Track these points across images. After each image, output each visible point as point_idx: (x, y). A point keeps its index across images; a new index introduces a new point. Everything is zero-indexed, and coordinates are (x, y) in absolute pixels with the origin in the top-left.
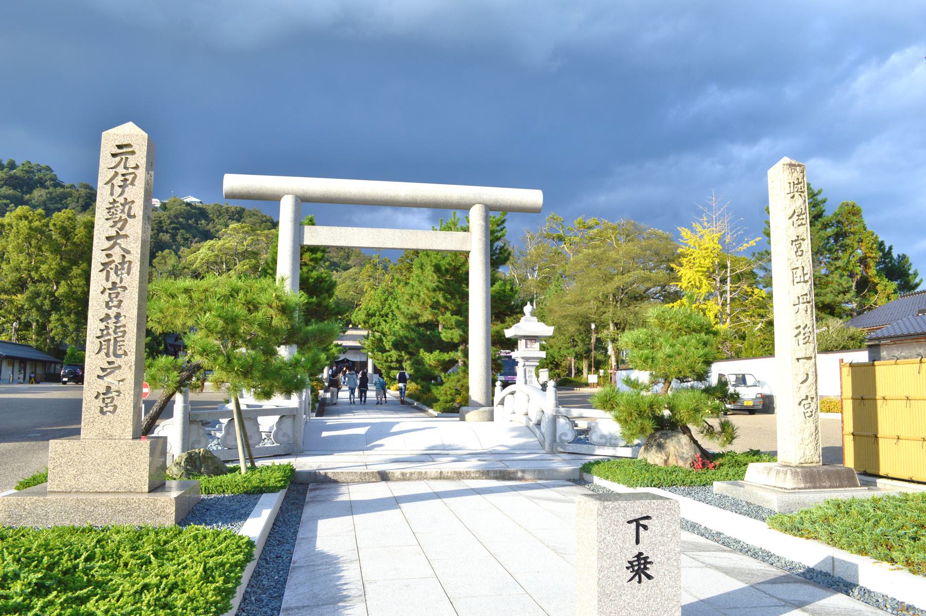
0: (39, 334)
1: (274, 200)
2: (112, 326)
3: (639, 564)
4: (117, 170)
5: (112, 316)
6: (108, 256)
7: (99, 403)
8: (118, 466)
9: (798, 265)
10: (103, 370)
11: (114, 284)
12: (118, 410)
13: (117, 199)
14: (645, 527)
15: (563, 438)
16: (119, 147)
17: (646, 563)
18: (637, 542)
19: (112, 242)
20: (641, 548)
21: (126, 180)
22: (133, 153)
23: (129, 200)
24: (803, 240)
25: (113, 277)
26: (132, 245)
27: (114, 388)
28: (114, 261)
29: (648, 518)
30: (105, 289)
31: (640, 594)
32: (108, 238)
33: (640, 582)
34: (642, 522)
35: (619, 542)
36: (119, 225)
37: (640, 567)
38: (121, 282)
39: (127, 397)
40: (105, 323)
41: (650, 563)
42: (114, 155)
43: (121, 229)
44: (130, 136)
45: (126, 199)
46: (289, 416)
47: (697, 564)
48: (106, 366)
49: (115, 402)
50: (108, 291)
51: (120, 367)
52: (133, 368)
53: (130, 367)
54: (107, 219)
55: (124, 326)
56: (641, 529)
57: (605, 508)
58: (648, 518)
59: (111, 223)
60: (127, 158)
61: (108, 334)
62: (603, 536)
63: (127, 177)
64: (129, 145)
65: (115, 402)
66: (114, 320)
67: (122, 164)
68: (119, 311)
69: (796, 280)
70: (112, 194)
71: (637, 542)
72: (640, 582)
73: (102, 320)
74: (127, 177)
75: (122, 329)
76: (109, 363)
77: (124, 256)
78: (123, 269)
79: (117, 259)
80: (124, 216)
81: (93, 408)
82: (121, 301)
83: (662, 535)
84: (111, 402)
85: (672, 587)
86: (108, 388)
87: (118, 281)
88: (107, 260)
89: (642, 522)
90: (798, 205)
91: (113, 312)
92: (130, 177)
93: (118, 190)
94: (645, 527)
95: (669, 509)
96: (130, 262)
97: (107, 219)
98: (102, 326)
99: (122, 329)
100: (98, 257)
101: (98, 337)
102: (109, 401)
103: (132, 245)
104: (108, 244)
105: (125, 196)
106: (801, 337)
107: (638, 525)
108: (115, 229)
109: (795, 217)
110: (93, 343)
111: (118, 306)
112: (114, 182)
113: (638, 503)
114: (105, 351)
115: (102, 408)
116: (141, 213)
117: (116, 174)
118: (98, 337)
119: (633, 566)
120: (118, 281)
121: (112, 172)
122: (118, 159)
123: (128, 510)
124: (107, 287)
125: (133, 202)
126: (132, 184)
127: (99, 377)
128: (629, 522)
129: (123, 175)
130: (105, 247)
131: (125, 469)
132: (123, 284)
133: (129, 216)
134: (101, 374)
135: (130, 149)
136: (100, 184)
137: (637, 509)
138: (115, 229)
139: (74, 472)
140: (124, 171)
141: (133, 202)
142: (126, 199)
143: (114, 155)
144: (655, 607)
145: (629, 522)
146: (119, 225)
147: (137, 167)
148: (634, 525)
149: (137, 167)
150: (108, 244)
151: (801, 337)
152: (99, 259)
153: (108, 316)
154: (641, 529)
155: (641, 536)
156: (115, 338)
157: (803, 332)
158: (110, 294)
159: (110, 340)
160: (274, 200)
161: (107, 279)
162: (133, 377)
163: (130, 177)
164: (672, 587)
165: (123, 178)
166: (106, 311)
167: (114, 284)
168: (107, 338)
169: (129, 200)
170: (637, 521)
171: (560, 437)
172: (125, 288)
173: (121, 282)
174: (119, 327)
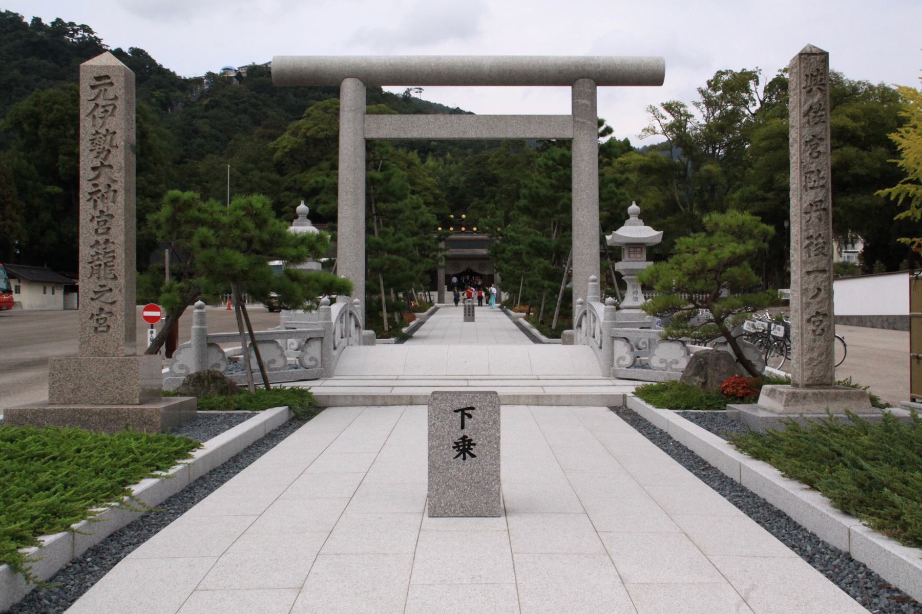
3: (464, 445)
5: (102, 242)
6: (95, 185)
8: (111, 380)
9: (813, 167)
10: (95, 292)
12: (111, 330)
13: (100, 131)
14: (470, 416)
15: (621, 362)
16: (98, 78)
17: (470, 444)
18: (463, 427)
20: (466, 432)
21: (106, 111)
22: (111, 84)
23: (111, 131)
24: (821, 139)
25: (100, 206)
26: (116, 174)
28: (100, 191)
29: (473, 408)
30: (93, 217)
31: (464, 469)
32: (94, 169)
33: (464, 459)
34: (467, 412)
36: (103, 156)
37: (464, 447)
38: (108, 210)
40: (95, 249)
41: (474, 444)
42: (93, 87)
43: (105, 159)
44: (108, 67)
45: (107, 130)
46: (317, 339)
49: (108, 323)
50: (96, 219)
51: (111, 290)
52: (123, 290)
53: (120, 290)
54: (91, 150)
55: (113, 251)
56: (466, 417)
58: (473, 408)
59: (95, 154)
60: (106, 90)
63: (107, 108)
64: (108, 77)
66: (104, 246)
67: (102, 96)
68: (107, 237)
69: (810, 185)
70: (94, 125)
71: (463, 427)
72: (464, 459)
73: (92, 246)
74: (107, 108)
75: (111, 254)
77: (109, 186)
80: (107, 147)
81: (88, 328)
82: (109, 229)
83: (484, 423)
85: (492, 465)
86: (101, 309)
88: (94, 190)
89: (467, 412)
90: (816, 100)
91: (102, 239)
92: (110, 109)
94: (470, 416)
95: (490, 402)
96: (115, 191)
97: (91, 150)
98: (93, 252)
99: (111, 254)
100: (85, 187)
101: (90, 263)
102: (102, 321)
103: (116, 174)
104: (93, 175)
106: (813, 248)
107: (463, 414)
109: (812, 114)
110: (85, 268)
112: (95, 113)
115: (96, 328)
117: (97, 105)
118: (90, 263)
119: (458, 447)
121: (93, 104)
122: (96, 91)
123: (119, 419)
125: (115, 133)
126: (112, 115)
127: (92, 299)
128: (456, 411)
129: (103, 107)
131: (118, 383)
132: (110, 212)
133: (111, 146)
134: (94, 296)
135: (108, 81)
139: (72, 387)
140: (104, 103)
141: (115, 133)
142: (107, 130)
143: (93, 87)
144: (477, 480)
145: (456, 411)
146: (103, 156)
147: (116, 98)
148: (459, 414)
149: (116, 98)
150: (93, 175)
151: (813, 248)
154: (466, 417)
157: (815, 242)
161: (95, 207)
164: (492, 465)
165: (102, 110)
167: (102, 212)
168: (97, 263)
169: (111, 131)
170: (462, 410)
171: (618, 362)
172: (112, 216)
173: (108, 210)
174: (109, 252)
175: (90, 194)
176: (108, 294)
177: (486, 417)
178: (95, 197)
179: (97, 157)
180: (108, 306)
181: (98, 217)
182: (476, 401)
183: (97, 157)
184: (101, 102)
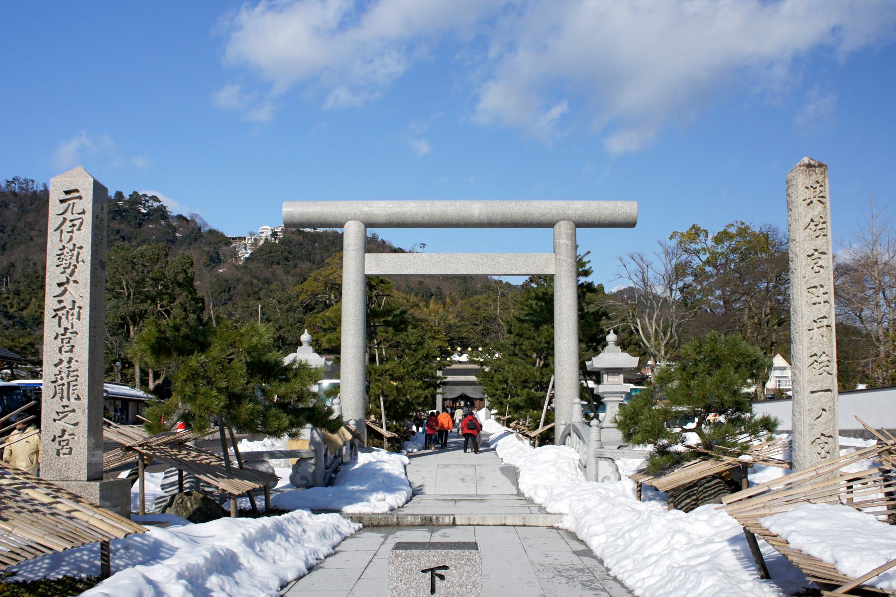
0: (666, 412)
1: (373, 284)
2: (65, 370)
4: (66, 216)
6: (60, 302)
7: (56, 445)
11: (66, 329)
13: (66, 245)
14: (442, 577)
16: (67, 193)
19: (62, 288)
22: (80, 198)
23: (78, 246)
27: (69, 431)
29: (445, 568)
30: (57, 335)
32: (60, 285)
34: (438, 572)
35: (412, 591)
36: (68, 271)
38: (72, 327)
39: (82, 440)
42: (62, 201)
47: (652, 567)
48: (61, 410)
49: (70, 445)
52: (86, 411)
54: (58, 266)
56: (437, 579)
57: (397, 556)
58: (445, 568)
59: (61, 269)
61: (62, 379)
62: (395, 584)
63: (74, 222)
64: (76, 191)
65: (70, 445)
70: (61, 241)
73: (56, 365)
75: (75, 373)
76: (64, 407)
78: (73, 315)
79: (67, 304)
81: (50, 451)
82: (73, 346)
83: (461, 586)
84: (67, 444)
86: (64, 431)
87: (70, 327)
88: (59, 306)
89: (438, 572)
91: (65, 356)
93: (66, 237)
94: (442, 577)
96: (80, 308)
97: (58, 266)
98: (56, 370)
99: (75, 373)
101: (53, 382)
104: (59, 290)
105: (73, 242)
108: (66, 275)
111: (71, 351)
112: (63, 228)
113: (433, 552)
114: (60, 395)
116: (89, 258)
117: (65, 219)
118: (53, 382)
120: (70, 327)
121: (61, 218)
122: (65, 205)
124: (59, 333)
128: (424, 571)
129: (71, 221)
130: (56, 294)
132: (74, 330)
134: (57, 417)
136: (50, 230)
137: (433, 558)
138: (66, 275)
141: (81, 248)
142: (74, 245)
143: (62, 201)
145: (424, 571)
148: (428, 575)
149: (83, 213)
150: (59, 290)
152: (51, 305)
153: (61, 361)
154: (437, 579)
155: (437, 586)
156: (69, 383)
158: (62, 339)
159: (63, 385)
160: (373, 284)
161: (60, 326)
162: (86, 420)
163: (77, 223)
165: (71, 224)
166: (60, 356)
167: (66, 329)
169: (78, 246)
170: (432, 570)
175: (55, 310)
176: (70, 414)
177: (464, 578)
178: (60, 313)
179: (63, 273)
180: (72, 427)
181: (62, 335)
182: (451, 559)
183: (63, 273)
184: (68, 216)
